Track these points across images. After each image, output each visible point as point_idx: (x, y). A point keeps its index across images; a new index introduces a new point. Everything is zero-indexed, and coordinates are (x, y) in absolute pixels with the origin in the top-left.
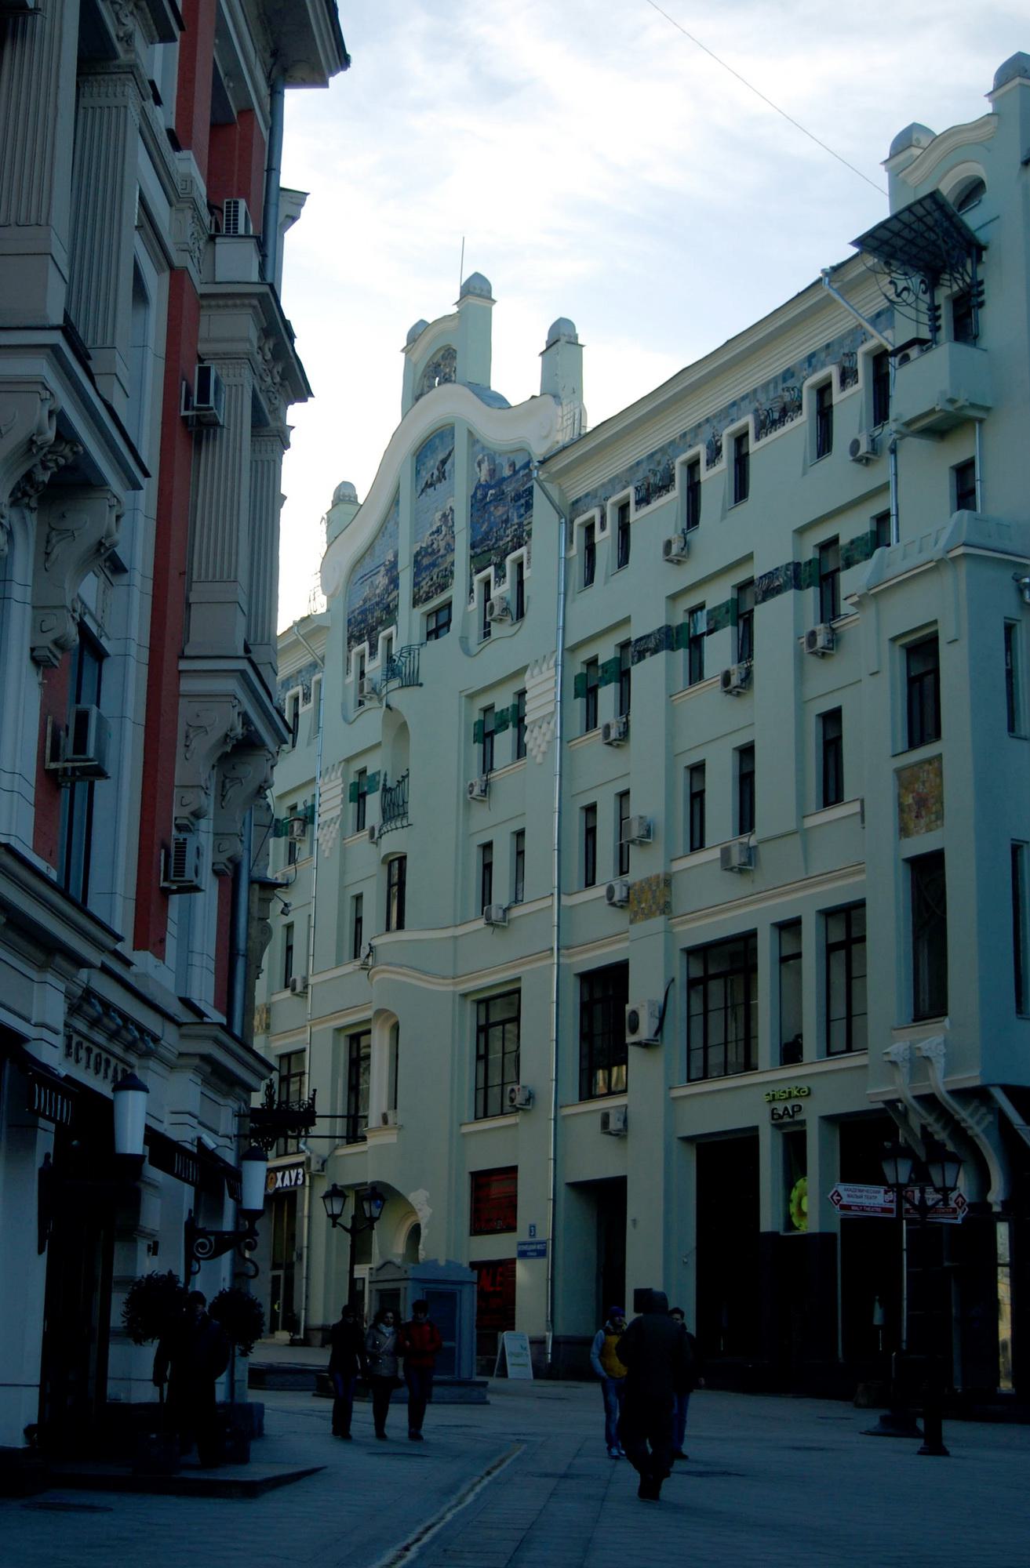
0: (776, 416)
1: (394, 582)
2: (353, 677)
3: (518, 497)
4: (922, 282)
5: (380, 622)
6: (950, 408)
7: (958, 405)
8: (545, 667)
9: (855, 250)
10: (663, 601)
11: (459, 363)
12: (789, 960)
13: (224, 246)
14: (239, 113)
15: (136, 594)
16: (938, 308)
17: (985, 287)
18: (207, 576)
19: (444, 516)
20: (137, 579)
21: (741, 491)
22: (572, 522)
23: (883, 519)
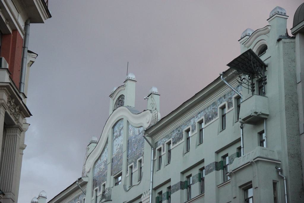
0: (210, 117)
2: (94, 197)
6: (256, 115)
7: (258, 114)
8: (147, 195)
9: (229, 67)
10: (214, 154)
11: (125, 100)
16: (254, 84)
17: (267, 78)
21: (201, 141)
22: (155, 149)
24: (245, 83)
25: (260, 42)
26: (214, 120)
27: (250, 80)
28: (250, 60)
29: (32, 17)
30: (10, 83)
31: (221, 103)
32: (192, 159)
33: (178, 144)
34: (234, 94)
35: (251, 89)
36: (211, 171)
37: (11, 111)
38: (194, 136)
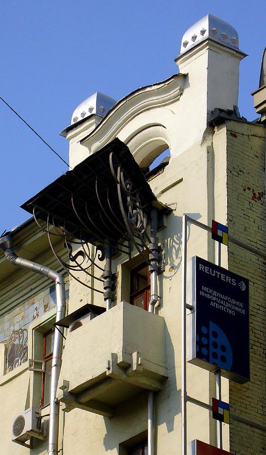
9: (27, 216)
24: (82, 269)
25: (146, 130)
27: (101, 259)
34: (34, 318)
35: (105, 291)
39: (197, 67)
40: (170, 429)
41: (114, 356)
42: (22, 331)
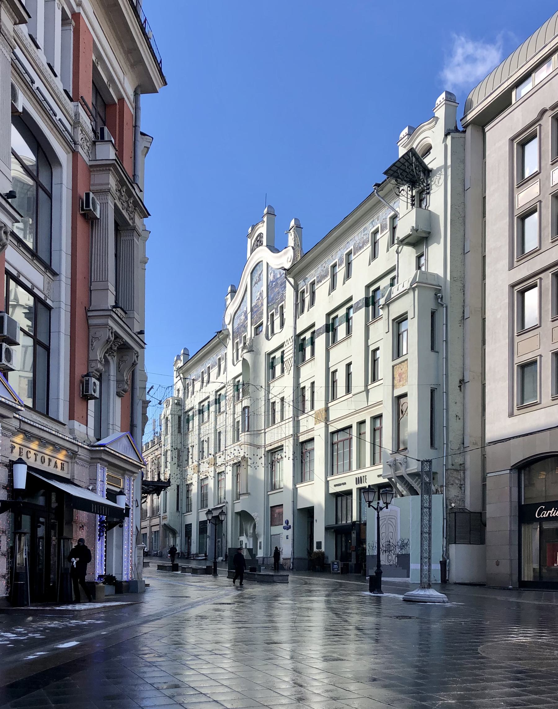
0: (361, 245)
1: (246, 318)
3: (281, 285)
4: (409, 187)
5: (243, 331)
9: (386, 177)
12: (360, 434)
13: (100, 147)
14: (118, 100)
15: (63, 285)
18: (97, 279)
19: (261, 293)
20: (63, 278)
23: (393, 279)
26: (365, 248)
28: (411, 164)
29: (145, 87)
30: (115, 160)
31: (374, 227)
32: (339, 297)
33: (323, 282)
36: (360, 308)
37: (122, 204)
38: (341, 272)
39: (440, 113)
40: (28, 326)
41: (413, 227)
42: (386, 218)
